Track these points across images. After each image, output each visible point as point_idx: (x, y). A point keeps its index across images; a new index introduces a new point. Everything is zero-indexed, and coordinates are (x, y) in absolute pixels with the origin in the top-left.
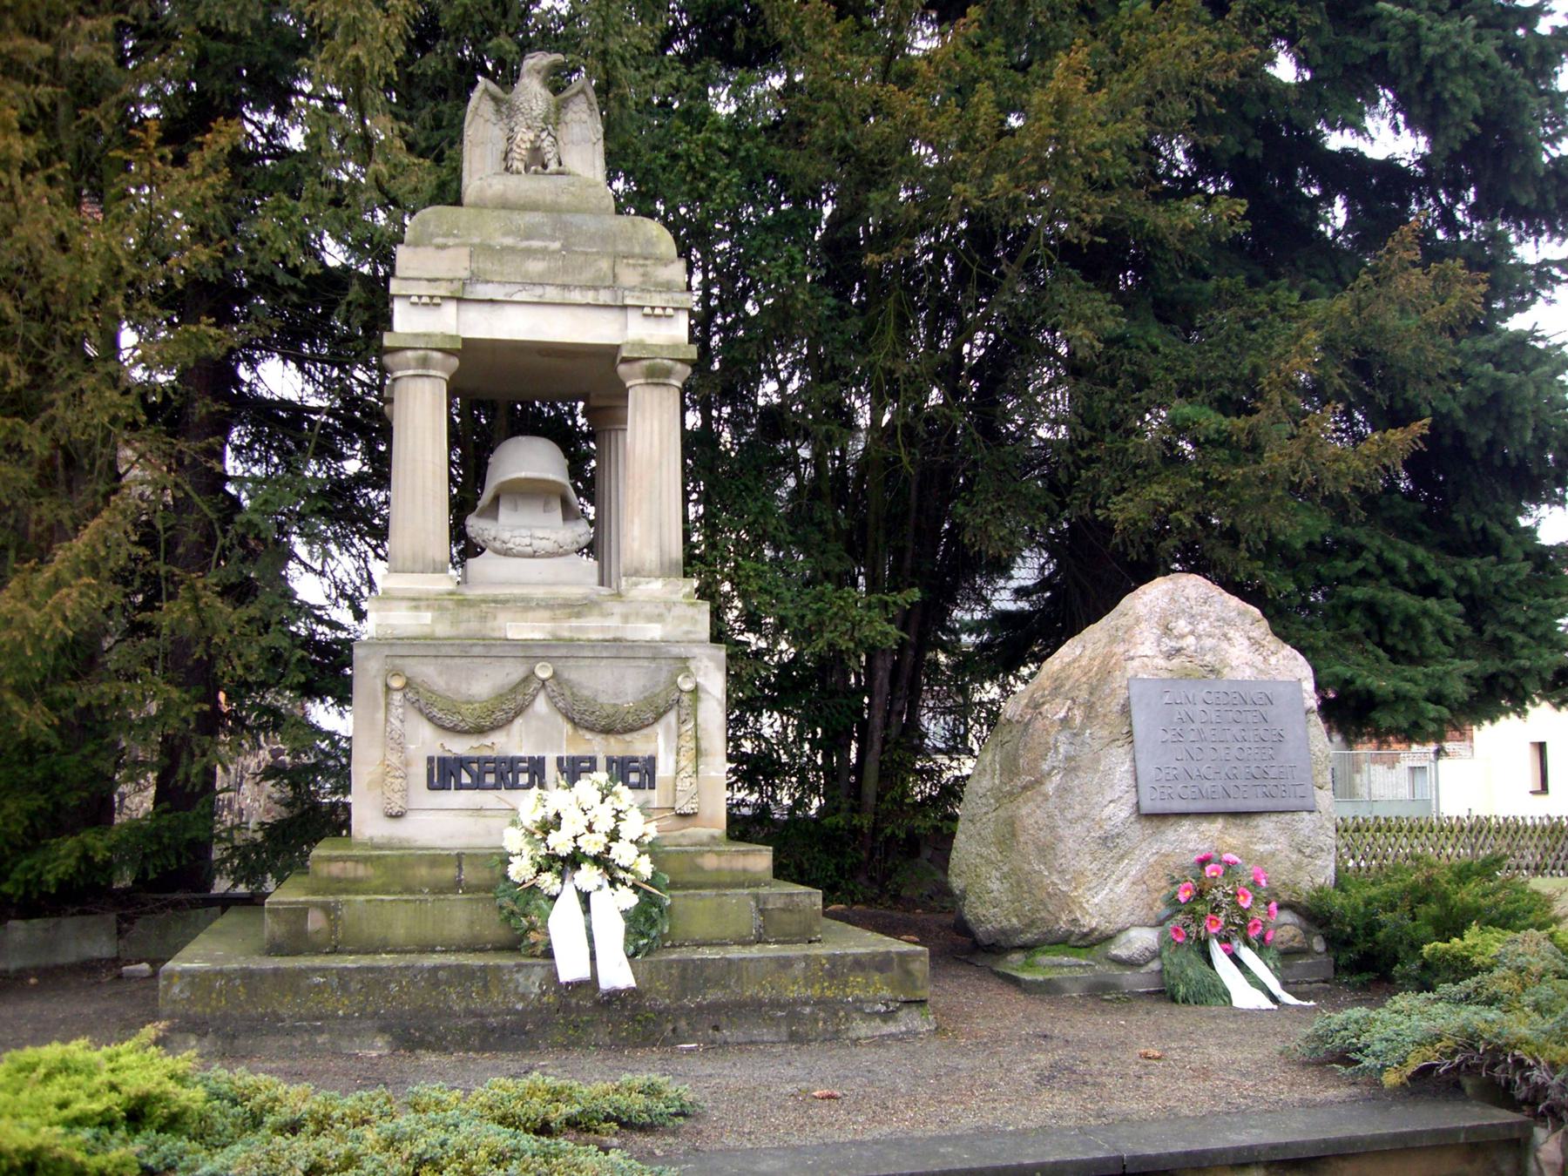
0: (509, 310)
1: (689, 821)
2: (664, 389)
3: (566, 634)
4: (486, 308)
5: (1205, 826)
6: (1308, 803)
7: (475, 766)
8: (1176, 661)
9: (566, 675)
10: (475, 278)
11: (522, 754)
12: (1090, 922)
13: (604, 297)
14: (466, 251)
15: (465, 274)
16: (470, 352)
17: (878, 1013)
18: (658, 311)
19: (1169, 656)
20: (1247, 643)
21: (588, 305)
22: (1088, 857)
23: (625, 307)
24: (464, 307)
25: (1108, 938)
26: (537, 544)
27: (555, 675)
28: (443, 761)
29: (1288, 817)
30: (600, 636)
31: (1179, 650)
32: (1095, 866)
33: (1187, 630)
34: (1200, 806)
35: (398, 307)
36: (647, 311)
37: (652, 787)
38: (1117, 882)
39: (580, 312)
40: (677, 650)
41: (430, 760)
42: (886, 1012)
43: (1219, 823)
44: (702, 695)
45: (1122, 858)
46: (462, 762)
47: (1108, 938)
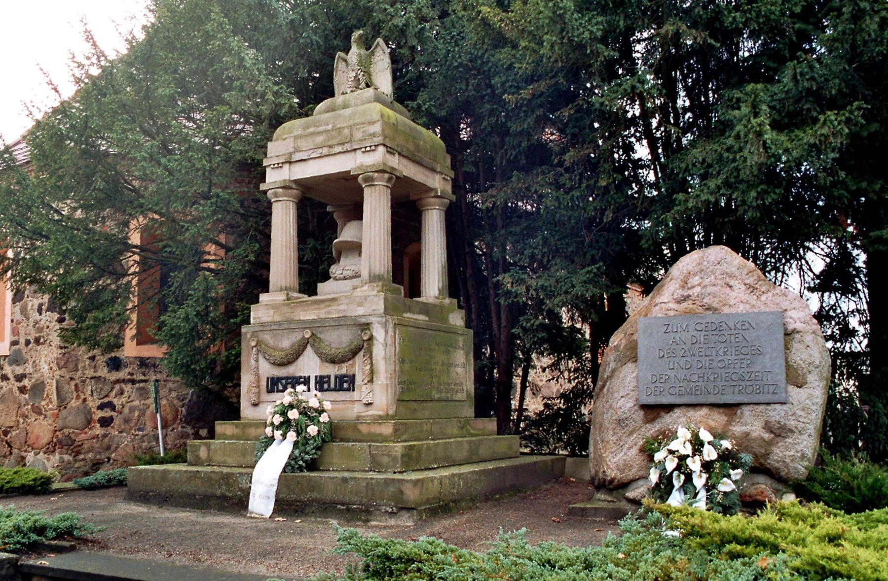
0: (311, 162)
1: (370, 408)
2: (373, 188)
3: (323, 316)
4: (303, 163)
5: (691, 413)
6: (782, 397)
7: (284, 381)
8: (685, 305)
9: (319, 336)
10: (297, 150)
11: (302, 375)
12: (612, 473)
13: (347, 147)
14: (292, 139)
15: (292, 150)
16: (301, 184)
17: (387, 512)
18: (368, 149)
19: (679, 302)
20: (743, 288)
21: (340, 152)
22: (611, 433)
23: (355, 150)
24: (293, 165)
25: (625, 485)
26: (345, 273)
27: (313, 334)
28: (272, 379)
29: (761, 407)
30: (337, 316)
31: (689, 296)
32: (614, 438)
33: (697, 283)
34: (693, 400)
35: (268, 171)
36: (363, 150)
37: (353, 390)
38: (629, 448)
39: (317, 160)
40: (363, 320)
41: (268, 378)
42: (391, 513)
43: (704, 411)
44: (375, 342)
45: (631, 433)
46: (279, 379)
47: (625, 485)
